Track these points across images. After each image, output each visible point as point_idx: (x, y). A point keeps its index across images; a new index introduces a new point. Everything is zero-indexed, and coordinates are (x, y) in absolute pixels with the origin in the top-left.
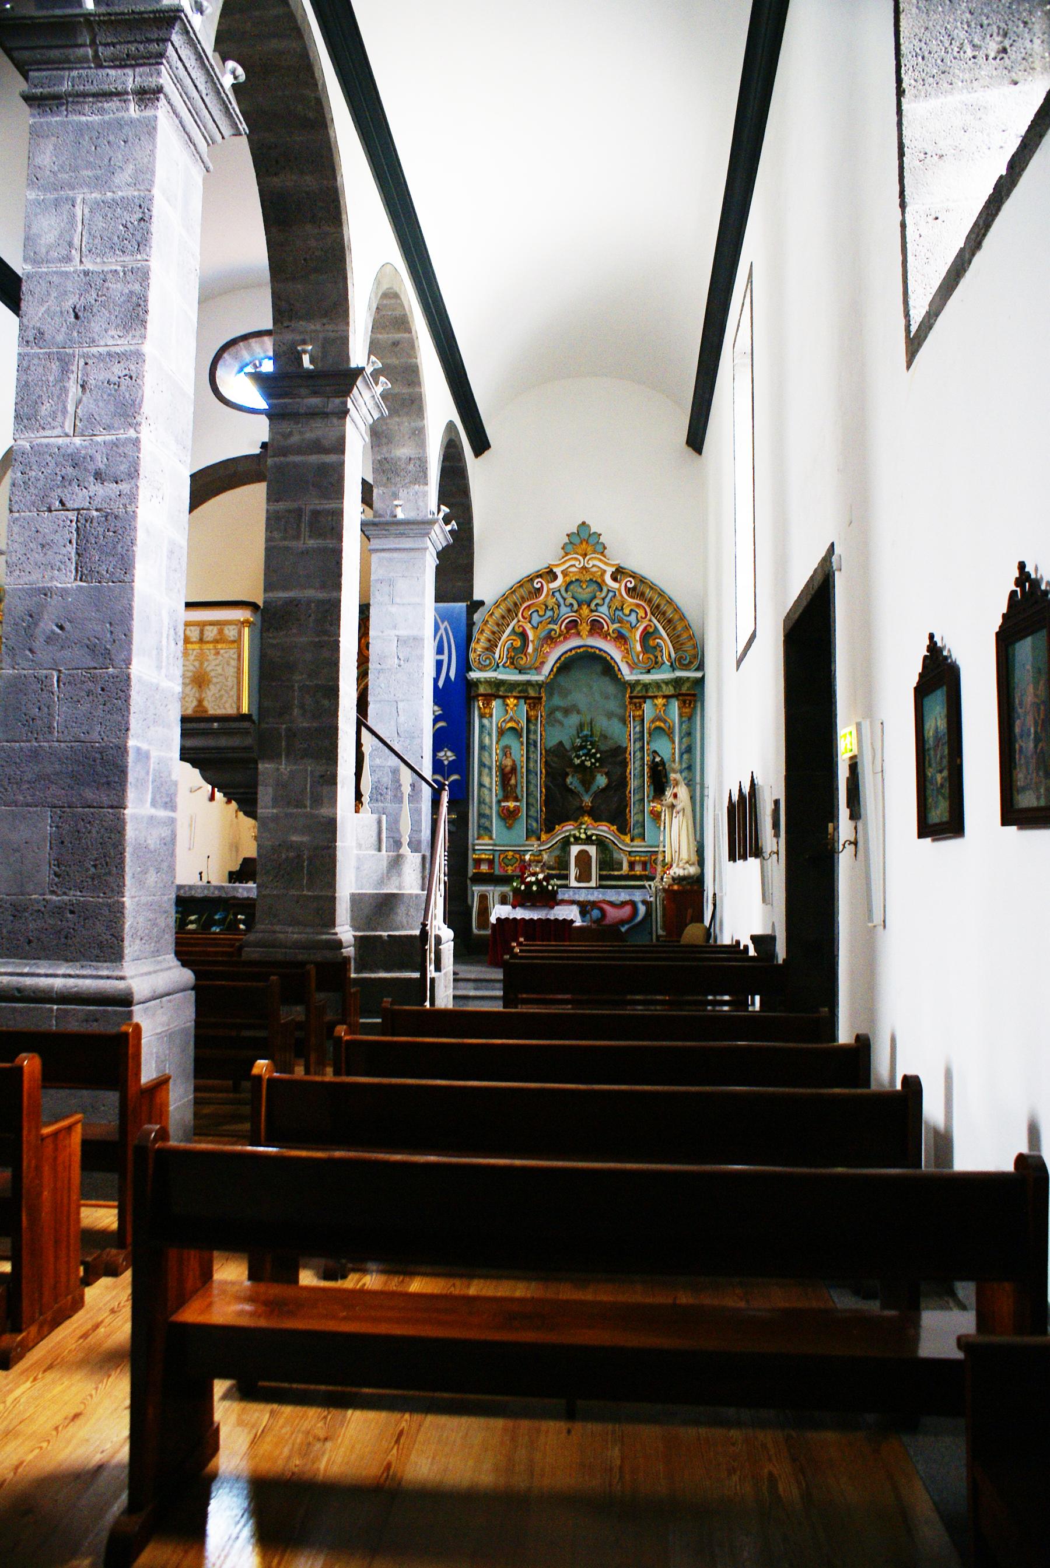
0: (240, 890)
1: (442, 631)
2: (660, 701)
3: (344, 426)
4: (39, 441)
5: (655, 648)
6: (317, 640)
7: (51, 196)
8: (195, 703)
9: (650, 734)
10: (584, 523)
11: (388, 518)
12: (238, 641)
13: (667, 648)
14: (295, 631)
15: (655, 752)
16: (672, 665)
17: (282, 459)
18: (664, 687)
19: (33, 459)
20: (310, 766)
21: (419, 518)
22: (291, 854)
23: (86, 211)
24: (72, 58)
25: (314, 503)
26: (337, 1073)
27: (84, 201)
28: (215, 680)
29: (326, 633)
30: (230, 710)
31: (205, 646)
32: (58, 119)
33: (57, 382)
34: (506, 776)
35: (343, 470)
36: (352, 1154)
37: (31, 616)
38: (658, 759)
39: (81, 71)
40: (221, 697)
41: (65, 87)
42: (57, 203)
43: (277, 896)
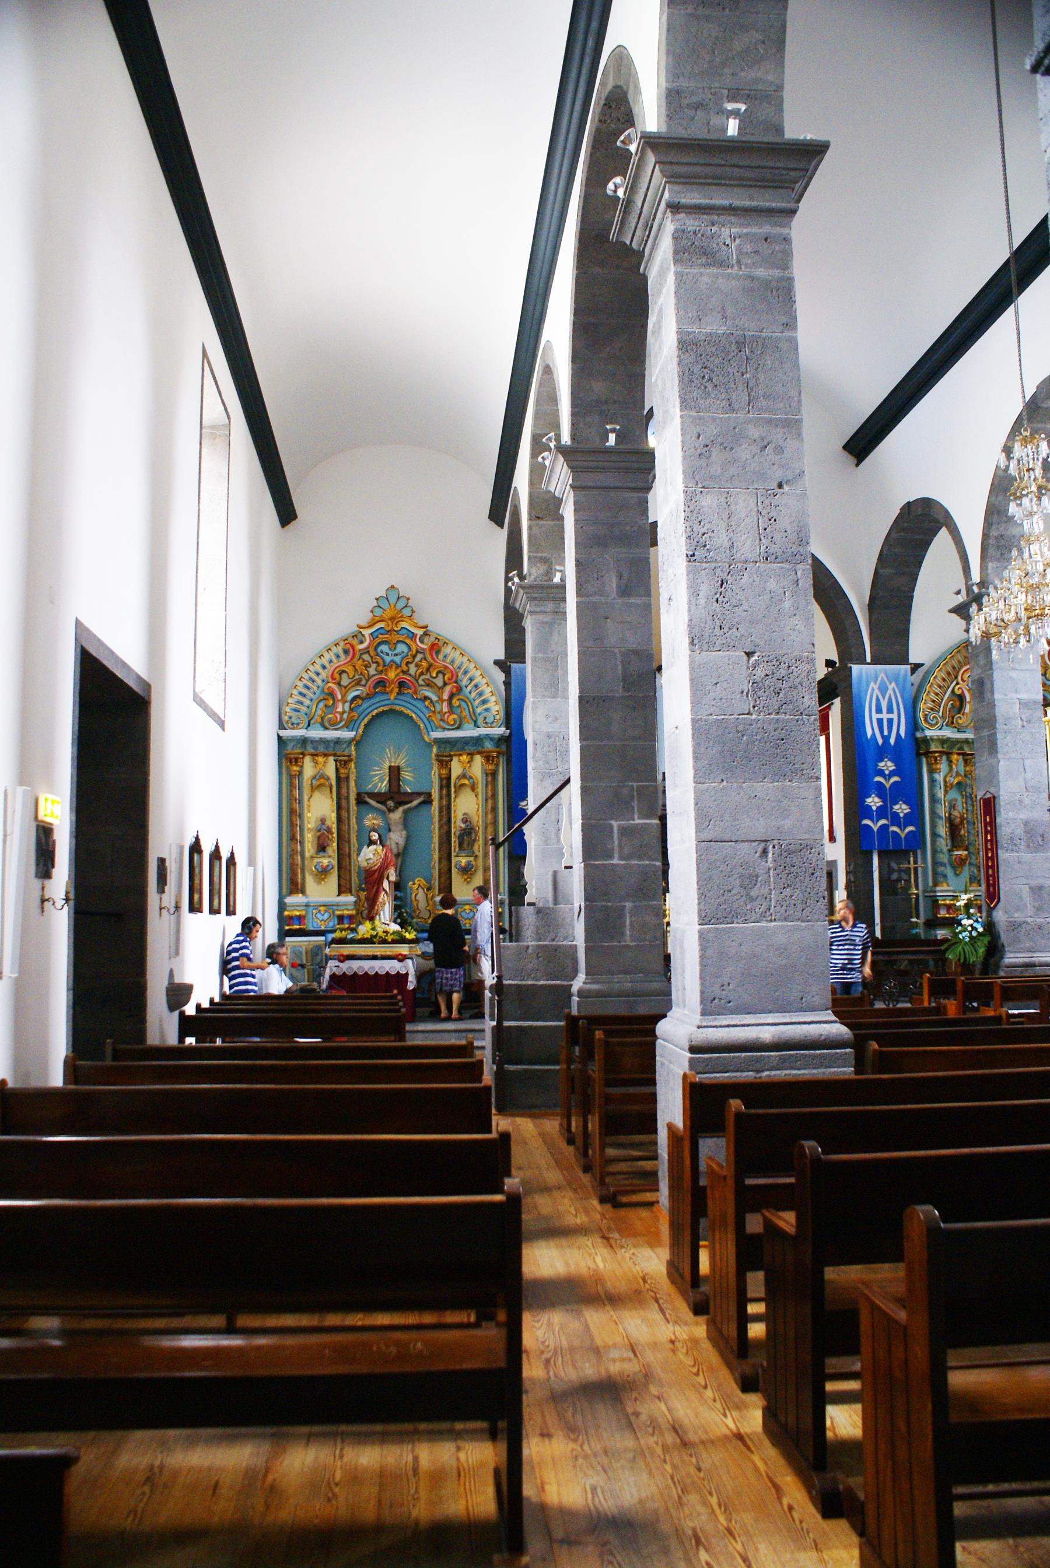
1: (890, 691)
10: (393, 587)
34: (954, 829)
36: (104, 1138)
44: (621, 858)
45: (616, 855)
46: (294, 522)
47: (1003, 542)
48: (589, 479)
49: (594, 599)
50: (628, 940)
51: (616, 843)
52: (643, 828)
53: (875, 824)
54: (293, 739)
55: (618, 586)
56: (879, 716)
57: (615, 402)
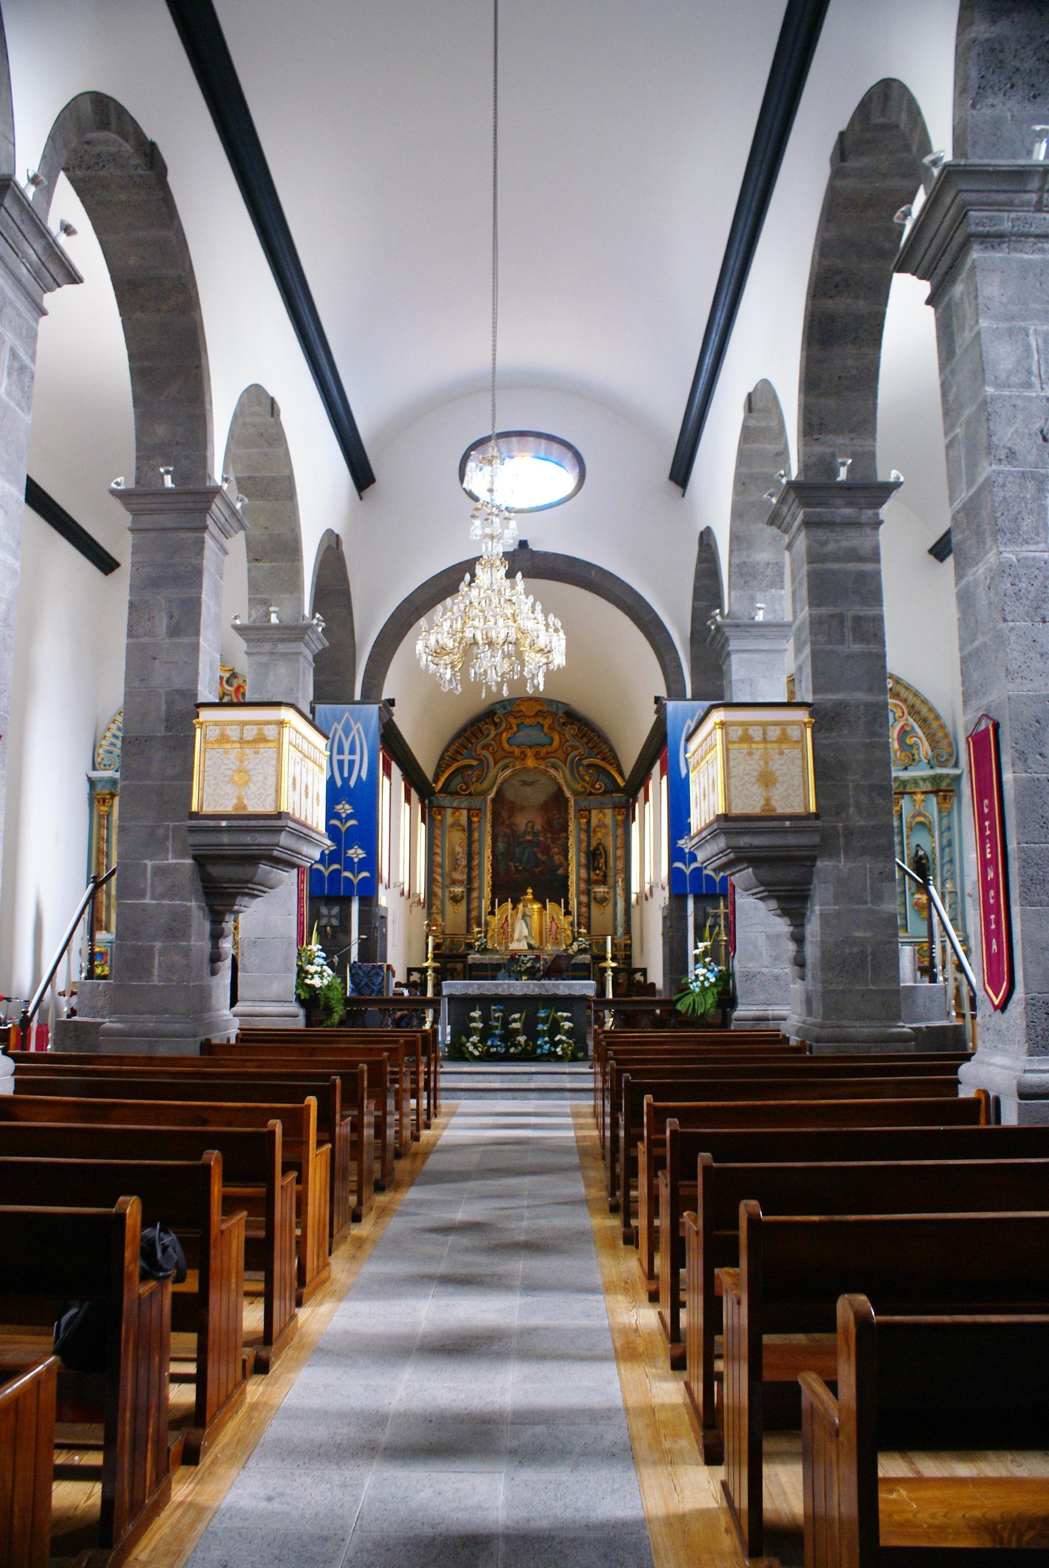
0: (561, 987)
1: (354, 732)
2: (919, 797)
3: (877, 536)
4: (1024, 554)
5: (912, 746)
6: (868, 741)
7: (1003, 325)
8: (763, 802)
9: (911, 828)
11: (746, 621)
12: (802, 740)
13: (925, 749)
14: (846, 732)
15: (918, 846)
16: (929, 763)
17: (820, 565)
18: (921, 783)
19: (1022, 571)
20: (867, 863)
21: (775, 621)
22: (855, 950)
23: (1040, 341)
24: (1017, 202)
25: (854, 610)
26: (707, 1169)
27: (1035, 330)
28: (780, 779)
29: (873, 734)
30: (799, 810)
31: (769, 746)
32: (1001, 255)
33: (1034, 499)
35: (880, 577)
37: (1038, 722)
38: (921, 853)
39: (1020, 214)
40: (788, 796)
41: (1006, 226)
42: (1011, 332)
43: (843, 991)
44: (153, 898)
45: (148, 894)
46: (116, 571)
47: (745, 570)
48: (147, 521)
49: (143, 640)
50: (156, 981)
51: (149, 882)
52: (176, 868)
53: (687, 867)
54: (101, 780)
55: (168, 627)
56: (341, 757)
57: (178, 444)
